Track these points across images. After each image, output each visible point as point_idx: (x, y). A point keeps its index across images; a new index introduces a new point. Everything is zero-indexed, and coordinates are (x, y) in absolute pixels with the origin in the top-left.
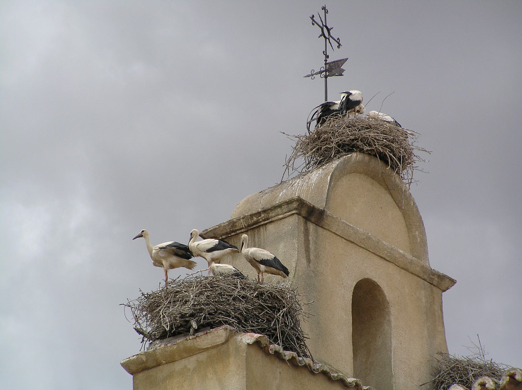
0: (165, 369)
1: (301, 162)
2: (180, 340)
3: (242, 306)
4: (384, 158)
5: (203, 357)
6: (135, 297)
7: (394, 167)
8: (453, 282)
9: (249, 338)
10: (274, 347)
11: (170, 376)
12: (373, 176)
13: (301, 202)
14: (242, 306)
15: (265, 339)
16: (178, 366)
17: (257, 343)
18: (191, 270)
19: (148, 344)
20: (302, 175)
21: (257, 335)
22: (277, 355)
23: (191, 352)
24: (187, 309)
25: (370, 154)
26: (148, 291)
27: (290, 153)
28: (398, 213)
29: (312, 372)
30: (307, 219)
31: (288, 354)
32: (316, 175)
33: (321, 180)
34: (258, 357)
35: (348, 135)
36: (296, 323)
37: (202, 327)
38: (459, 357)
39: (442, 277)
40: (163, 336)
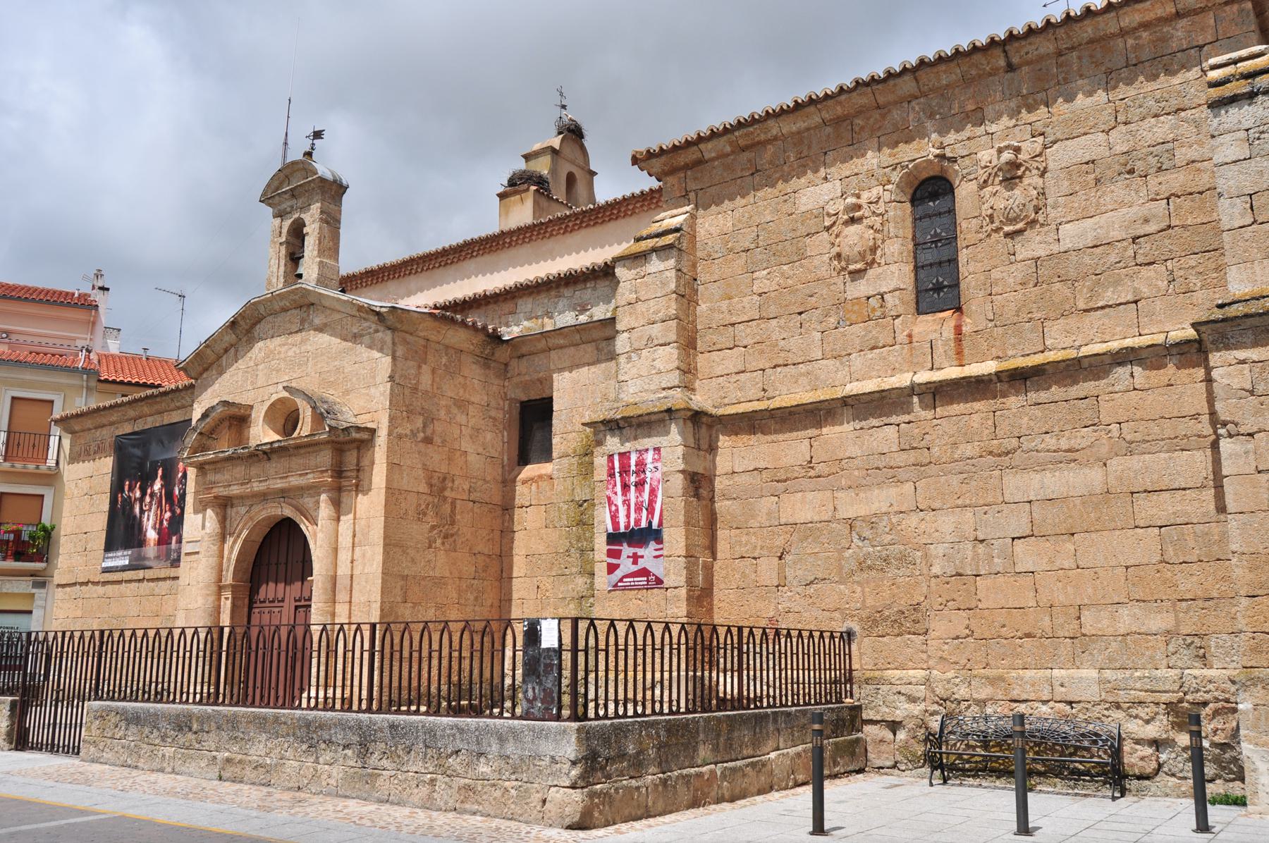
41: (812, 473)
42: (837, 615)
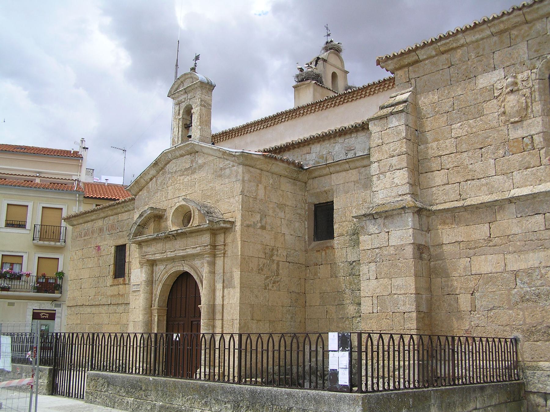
0: (300, 87)
1: (323, 51)
2: (302, 82)
3: (313, 76)
4: (337, 51)
5: (306, 85)
6: (295, 75)
7: (339, 52)
8: (377, 65)
9: (314, 82)
10: (318, 83)
11: (301, 88)
12: (335, 54)
13: (323, 58)
14: (313, 76)
15: (317, 82)
16: (302, 87)
17: (315, 83)
18: (262, 149)
19: (113, 250)
20: (323, 54)
21: (315, 81)
22: (319, 85)
23: (304, 84)
24: (303, 77)
25: (335, 50)
26: (297, 74)
27: (321, 50)
28: (340, 60)
29: (328, 89)
30: (324, 61)
31: (321, 85)
32: (325, 54)
33: (326, 54)
34: (315, 85)
35: (331, 47)
36: (322, 79)
37: (306, 80)
38: (350, 85)
39: (347, 71)
40: (299, 82)
41: (491, 244)
42: (508, 328)
